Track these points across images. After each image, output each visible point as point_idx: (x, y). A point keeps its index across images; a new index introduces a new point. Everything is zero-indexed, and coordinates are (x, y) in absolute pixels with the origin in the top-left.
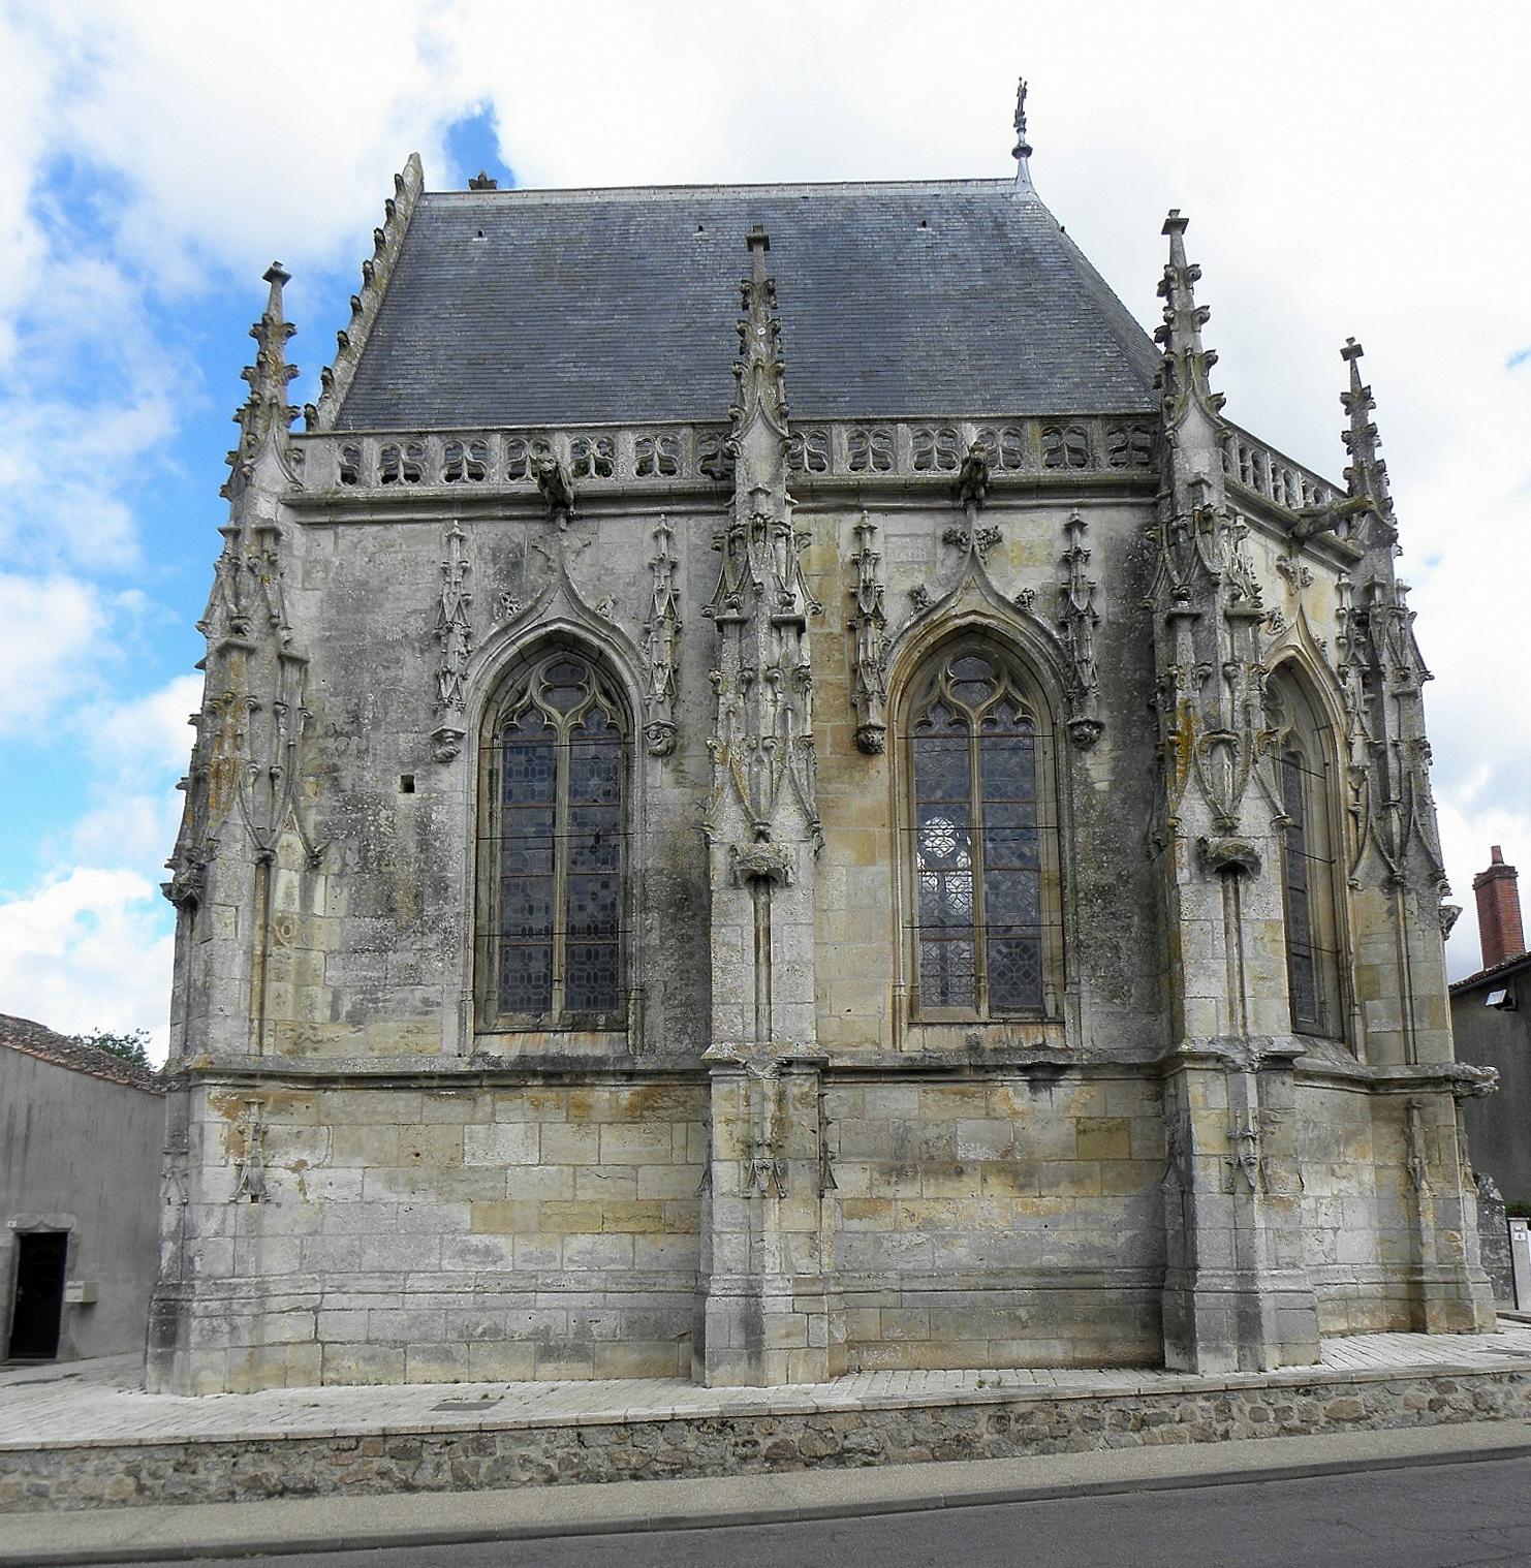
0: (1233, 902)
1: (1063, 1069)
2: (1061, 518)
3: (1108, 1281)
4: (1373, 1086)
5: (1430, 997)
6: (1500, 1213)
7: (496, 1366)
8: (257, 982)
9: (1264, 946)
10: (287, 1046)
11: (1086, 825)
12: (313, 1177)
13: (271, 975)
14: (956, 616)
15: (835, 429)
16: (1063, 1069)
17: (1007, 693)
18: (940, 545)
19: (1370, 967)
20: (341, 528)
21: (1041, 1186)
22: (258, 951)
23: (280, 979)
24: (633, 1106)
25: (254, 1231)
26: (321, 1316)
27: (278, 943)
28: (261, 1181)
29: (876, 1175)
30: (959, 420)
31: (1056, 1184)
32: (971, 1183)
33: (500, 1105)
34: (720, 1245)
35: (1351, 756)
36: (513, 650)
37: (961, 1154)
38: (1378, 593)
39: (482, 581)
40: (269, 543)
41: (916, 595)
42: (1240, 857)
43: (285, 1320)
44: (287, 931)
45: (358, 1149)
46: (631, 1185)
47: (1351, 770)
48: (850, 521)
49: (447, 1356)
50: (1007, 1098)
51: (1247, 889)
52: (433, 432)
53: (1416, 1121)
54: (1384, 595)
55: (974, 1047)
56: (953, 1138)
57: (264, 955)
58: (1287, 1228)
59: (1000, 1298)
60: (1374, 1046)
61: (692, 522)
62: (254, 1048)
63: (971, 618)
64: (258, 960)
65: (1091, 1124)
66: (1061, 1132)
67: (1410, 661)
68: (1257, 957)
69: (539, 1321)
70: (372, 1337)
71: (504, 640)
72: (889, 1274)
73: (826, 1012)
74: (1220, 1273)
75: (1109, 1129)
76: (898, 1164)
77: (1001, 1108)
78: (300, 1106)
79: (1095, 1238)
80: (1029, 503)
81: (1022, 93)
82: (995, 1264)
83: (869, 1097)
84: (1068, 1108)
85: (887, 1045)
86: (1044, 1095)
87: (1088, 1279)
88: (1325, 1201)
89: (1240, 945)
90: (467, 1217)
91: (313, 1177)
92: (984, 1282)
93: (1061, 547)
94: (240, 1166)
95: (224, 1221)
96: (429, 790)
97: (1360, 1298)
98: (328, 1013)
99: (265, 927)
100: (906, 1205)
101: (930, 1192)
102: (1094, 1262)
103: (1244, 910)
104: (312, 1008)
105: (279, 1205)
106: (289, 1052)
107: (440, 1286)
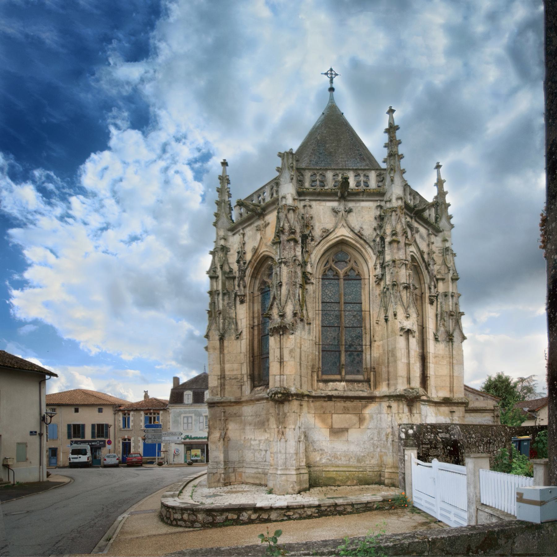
15: (307, 171)
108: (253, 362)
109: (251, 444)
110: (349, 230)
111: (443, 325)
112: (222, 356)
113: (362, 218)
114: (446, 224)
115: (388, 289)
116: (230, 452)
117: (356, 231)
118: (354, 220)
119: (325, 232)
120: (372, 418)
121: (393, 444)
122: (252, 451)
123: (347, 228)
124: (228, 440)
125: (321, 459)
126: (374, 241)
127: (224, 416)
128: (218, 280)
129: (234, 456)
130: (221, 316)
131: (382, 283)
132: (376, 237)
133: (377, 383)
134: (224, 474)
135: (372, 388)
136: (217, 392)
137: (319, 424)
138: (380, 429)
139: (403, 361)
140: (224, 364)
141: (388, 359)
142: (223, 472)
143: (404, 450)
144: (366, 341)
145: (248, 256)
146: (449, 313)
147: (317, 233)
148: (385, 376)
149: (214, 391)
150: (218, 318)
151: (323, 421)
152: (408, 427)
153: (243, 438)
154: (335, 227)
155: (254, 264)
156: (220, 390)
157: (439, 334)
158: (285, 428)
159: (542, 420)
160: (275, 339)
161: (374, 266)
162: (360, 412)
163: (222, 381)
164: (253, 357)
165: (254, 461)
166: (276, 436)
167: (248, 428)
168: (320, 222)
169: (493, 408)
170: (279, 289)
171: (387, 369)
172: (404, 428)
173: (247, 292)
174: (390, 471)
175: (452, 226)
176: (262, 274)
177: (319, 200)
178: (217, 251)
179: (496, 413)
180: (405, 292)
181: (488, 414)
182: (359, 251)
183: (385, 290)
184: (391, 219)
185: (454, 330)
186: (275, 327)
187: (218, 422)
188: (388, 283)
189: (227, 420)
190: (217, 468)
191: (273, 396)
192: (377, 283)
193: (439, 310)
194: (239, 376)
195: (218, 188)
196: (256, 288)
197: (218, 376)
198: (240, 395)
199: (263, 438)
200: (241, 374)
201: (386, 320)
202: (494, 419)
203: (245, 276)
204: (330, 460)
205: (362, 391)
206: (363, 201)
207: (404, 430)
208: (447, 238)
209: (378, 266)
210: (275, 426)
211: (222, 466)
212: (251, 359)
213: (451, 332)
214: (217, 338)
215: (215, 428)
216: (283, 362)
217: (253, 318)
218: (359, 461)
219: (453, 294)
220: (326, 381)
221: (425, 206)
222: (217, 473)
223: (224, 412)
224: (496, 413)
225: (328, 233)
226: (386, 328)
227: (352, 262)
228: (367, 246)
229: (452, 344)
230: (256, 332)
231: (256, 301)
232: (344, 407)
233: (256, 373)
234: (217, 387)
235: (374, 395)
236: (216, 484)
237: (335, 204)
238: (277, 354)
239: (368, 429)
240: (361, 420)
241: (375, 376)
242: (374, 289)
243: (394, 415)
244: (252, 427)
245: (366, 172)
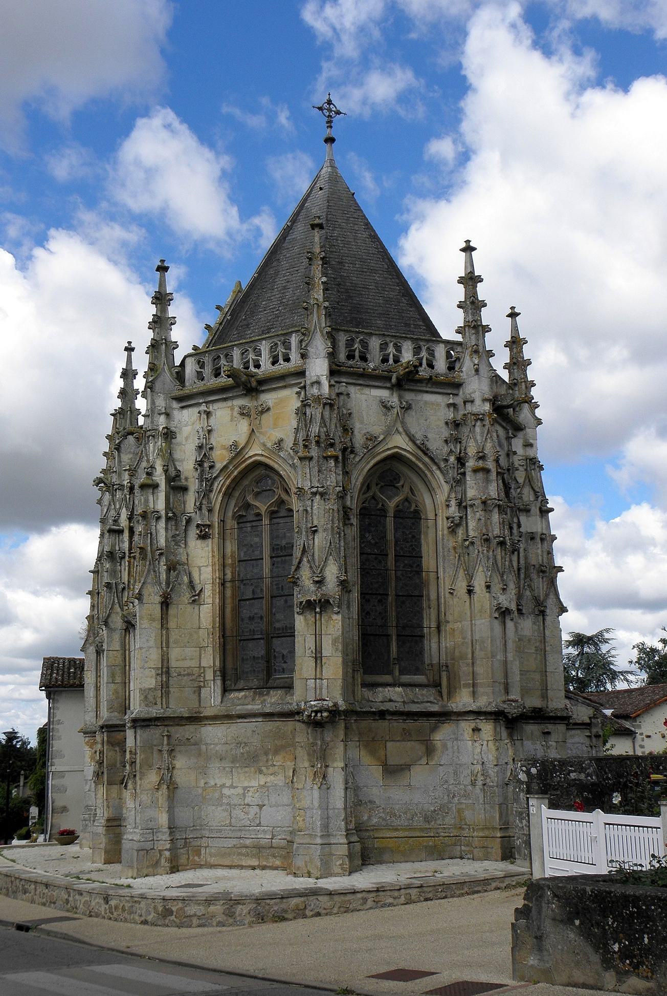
15: (341, 333)
52: (376, 334)
63: (396, 450)
80: (377, 384)
88: (251, 789)
97: (272, 847)
108: (224, 645)
109: (222, 795)
110: (407, 439)
111: (530, 586)
112: (164, 632)
113: (426, 420)
114: (529, 415)
115: (472, 543)
116: (176, 810)
117: (418, 442)
118: (415, 424)
119: (371, 440)
120: (445, 746)
121: (484, 790)
122: (224, 807)
123: (404, 436)
124: (175, 788)
125: (370, 817)
126: (446, 460)
127: (168, 744)
128: (156, 491)
129: (184, 816)
130: (163, 559)
131: (460, 532)
132: (448, 455)
133: (452, 689)
134: (169, 850)
135: (445, 697)
136: (155, 698)
137: (366, 759)
138: (458, 766)
139: (498, 657)
140: (168, 647)
141: (473, 653)
142: (168, 846)
143: (528, 798)
144: (429, 621)
145: (220, 457)
146: (537, 566)
147: (359, 440)
148: (465, 679)
149: (151, 698)
150: (157, 562)
151: (373, 752)
152: (529, 764)
153: (202, 783)
154: (388, 434)
155: (233, 472)
156: (160, 695)
157: (523, 602)
158: (327, 766)
159: (649, 737)
160: (306, 620)
161: (447, 501)
162: (428, 738)
163: (164, 679)
164: (223, 636)
166: (309, 781)
167: (215, 765)
168: (362, 423)
169: (588, 721)
170: (311, 537)
171: (475, 669)
172: (525, 766)
173: (216, 520)
174: (481, 834)
175: (539, 422)
176: (244, 490)
177: (360, 385)
178: (153, 436)
179: (594, 730)
180: (499, 550)
181: (578, 732)
182: (422, 475)
183: (467, 543)
184: (474, 432)
185: (547, 595)
186: (310, 600)
187: (156, 755)
188: (471, 533)
189: (172, 750)
190: (153, 840)
191: (313, 715)
192: (450, 530)
193: (522, 561)
194: (196, 671)
196: (230, 514)
197: (158, 669)
198: (197, 705)
199: (254, 783)
200: (200, 667)
201: (470, 592)
202: (591, 740)
203: (211, 491)
204: (384, 820)
205: (428, 701)
206: (427, 392)
207: (524, 769)
208: (531, 441)
209: (453, 503)
210: (307, 764)
211: (166, 837)
212: (222, 640)
213: (542, 598)
214: (158, 599)
215: (150, 766)
216: (321, 657)
217: (224, 566)
218: (427, 819)
219: (544, 536)
220: (373, 686)
221: (512, 402)
222: (153, 849)
223: (169, 737)
224: (594, 730)
225: (376, 443)
226: (468, 603)
227: (406, 489)
228: (434, 468)
229: (544, 620)
230: (229, 593)
231: (228, 536)
232: (404, 729)
233: (229, 665)
234: (155, 689)
235: (447, 709)
236: (151, 869)
237: (384, 394)
238: (311, 643)
239: (440, 765)
240: (430, 751)
241: (449, 679)
242: (446, 538)
243: (485, 743)
245: (430, 344)
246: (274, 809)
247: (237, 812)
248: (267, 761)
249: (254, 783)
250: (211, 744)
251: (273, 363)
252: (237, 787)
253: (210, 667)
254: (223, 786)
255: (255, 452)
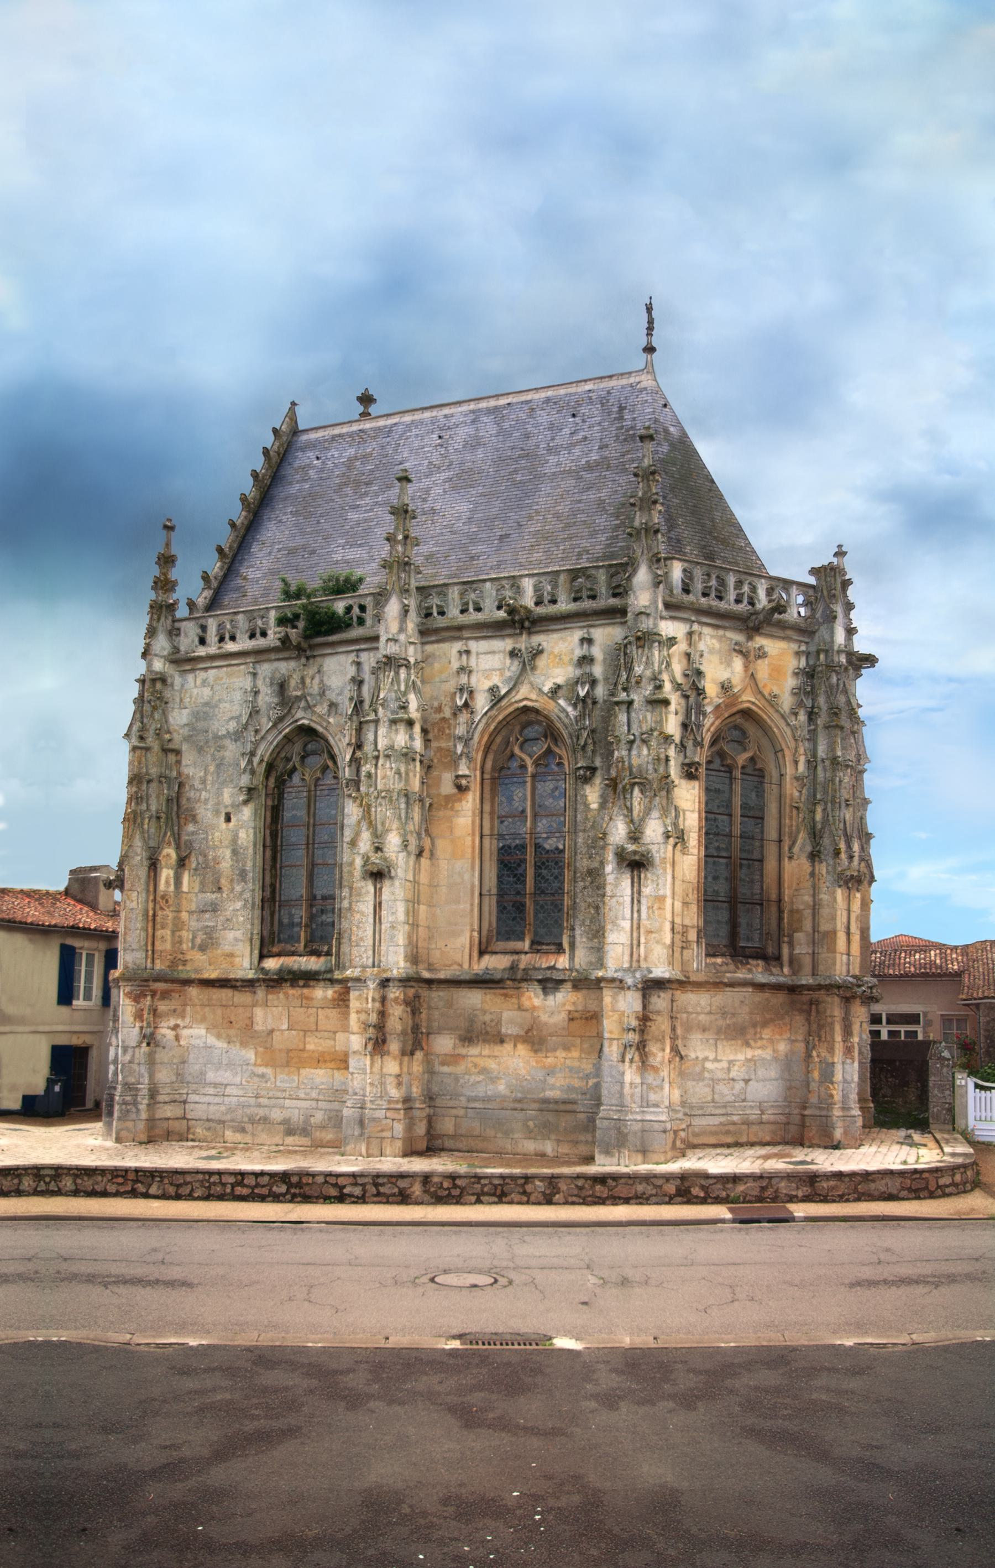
0: (637, 886)
1: (562, 981)
2: (578, 634)
3: (580, 1108)
4: (793, 989)
5: (828, 932)
6: (948, 1066)
7: (265, 1136)
8: (150, 930)
9: (653, 912)
10: (168, 963)
11: (584, 831)
12: (185, 1032)
13: (158, 926)
14: (516, 702)
16: (562, 981)
17: (549, 747)
18: (508, 657)
19: (798, 911)
20: (198, 672)
21: (547, 1051)
22: (151, 913)
23: (163, 928)
24: (334, 1000)
25: (151, 1062)
26: (187, 1106)
27: (162, 909)
28: (152, 1034)
29: (457, 1041)
30: (521, 576)
31: (555, 1050)
32: (508, 1047)
33: (270, 997)
34: (352, 1080)
35: (797, 769)
36: (281, 737)
37: (503, 1030)
38: (822, 657)
39: (267, 697)
40: (159, 686)
41: (493, 690)
42: (637, 858)
43: (167, 1107)
44: (167, 901)
45: (203, 1019)
46: (332, 1042)
47: (797, 779)
48: (458, 646)
49: (243, 1130)
50: (530, 998)
51: (646, 876)
53: (814, 1013)
54: (826, 657)
55: (513, 968)
56: (499, 1022)
57: (154, 915)
58: (655, 1083)
59: (519, 1115)
60: (794, 962)
61: (372, 654)
62: (149, 965)
64: (150, 918)
65: (576, 1015)
66: (561, 1017)
67: (842, 699)
68: (649, 918)
69: (286, 1114)
70: (210, 1117)
71: (275, 732)
72: (462, 1098)
73: (433, 946)
74: (614, 1108)
75: (587, 1019)
76: (469, 1035)
77: (526, 1003)
78: (175, 995)
79: (577, 1083)
81: (649, 309)
82: (519, 1095)
83: (455, 996)
84: (564, 1005)
85: (466, 966)
86: (551, 998)
87: (569, 1107)
89: (639, 911)
90: (253, 1057)
91: (185, 1032)
92: (512, 1105)
93: (578, 653)
94: (142, 1028)
95: (133, 1055)
96: (238, 820)
97: (761, 1123)
98: (190, 945)
99: (155, 900)
100: (473, 1059)
101: (486, 1052)
102: (573, 1096)
103: (643, 889)
104: (180, 942)
105: (164, 1048)
106: (169, 966)
107: (241, 1093)
109: (704, 1068)
122: (706, 1082)
143: (953, 1073)
165: (713, 1101)
195: (870, 762)
199: (741, 1057)
238: (845, 920)
244: (710, 1035)
246: (761, 1084)
247: (721, 1087)
248: (755, 1034)
249: (741, 1057)
250: (692, 1013)
251: (462, 612)
252: (721, 1061)
253: (693, 927)
254: (706, 1059)
255: (525, 694)
